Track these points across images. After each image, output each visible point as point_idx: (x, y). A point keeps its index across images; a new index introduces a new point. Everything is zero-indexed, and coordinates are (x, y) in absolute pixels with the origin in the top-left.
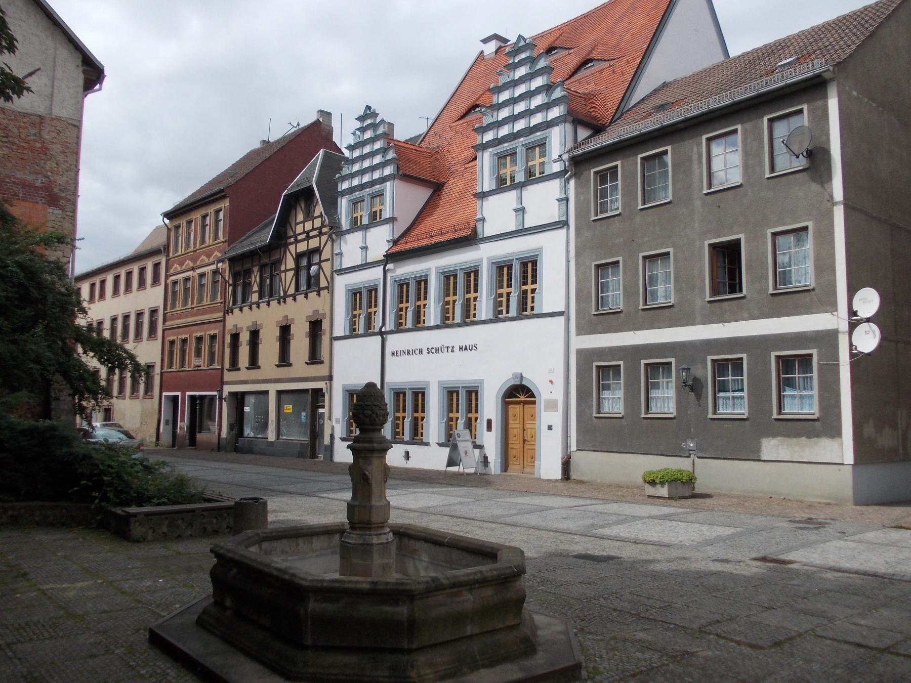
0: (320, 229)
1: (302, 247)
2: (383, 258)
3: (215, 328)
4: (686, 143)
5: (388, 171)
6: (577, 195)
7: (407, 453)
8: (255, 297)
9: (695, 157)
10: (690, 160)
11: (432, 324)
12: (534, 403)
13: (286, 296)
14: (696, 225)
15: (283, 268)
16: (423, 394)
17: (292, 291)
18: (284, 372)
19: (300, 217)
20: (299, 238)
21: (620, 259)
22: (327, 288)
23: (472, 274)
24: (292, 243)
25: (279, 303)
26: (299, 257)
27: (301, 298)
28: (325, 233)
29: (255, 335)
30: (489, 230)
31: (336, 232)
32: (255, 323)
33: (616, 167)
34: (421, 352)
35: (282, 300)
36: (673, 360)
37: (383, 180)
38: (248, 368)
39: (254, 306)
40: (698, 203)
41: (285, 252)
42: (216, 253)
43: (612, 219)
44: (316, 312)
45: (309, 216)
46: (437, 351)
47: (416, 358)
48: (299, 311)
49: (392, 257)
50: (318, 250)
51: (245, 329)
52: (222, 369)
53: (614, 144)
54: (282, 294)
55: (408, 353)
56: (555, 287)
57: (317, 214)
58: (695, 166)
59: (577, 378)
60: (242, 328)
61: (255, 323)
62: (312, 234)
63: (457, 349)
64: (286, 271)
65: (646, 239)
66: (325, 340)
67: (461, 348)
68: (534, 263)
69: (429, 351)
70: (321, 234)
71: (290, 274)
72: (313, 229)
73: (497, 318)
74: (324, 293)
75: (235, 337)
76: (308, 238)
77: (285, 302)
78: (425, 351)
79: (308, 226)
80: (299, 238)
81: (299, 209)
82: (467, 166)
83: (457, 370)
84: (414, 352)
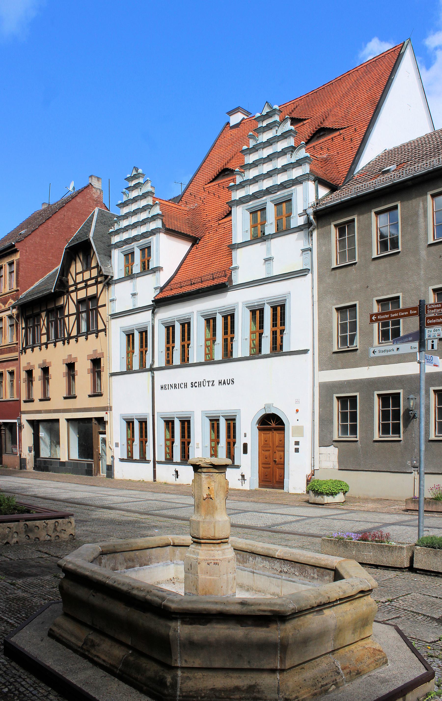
0: (96, 278)
1: (82, 294)
2: (152, 303)
3: (13, 366)
4: (414, 200)
5: (158, 224)
6: (319, 245)
7: (177, 472)
8: (44, 339)
9: (421, 211)
10: (416, 214)
11: (195, 362)
12: (283, 429)
13: (70, 338)
14: (422, 272)
15: (66, 313)
16: (189, 422)
17: (74, 333)
18: (70, 404)
19: (79, 267)
20: (79, 286)
21: (357, 303)
22: (104, 330)
23: (229, 318)
24: (73, 291)
25: (64, 344)
26: (81, 302)
27: (51, 346)
28: (101, 282)
29: (45, 370)
30: (239, 278)
31: (108, 282)
32: (44, 362)
33: (353, 220)
34: (186, 386)
35: (67, 340)
36: (401, 391)
37: (153, 232)
38: (41, 400)
39: (43, 347)
40: (423, 253)
41: (68, 298)
42: (11, 300)
43: (350, 268)
44: (95, 351)
45: (87, 267)
46: (200, 385)
47: (206, 389)
48: (81, 351)
49: (160, 303)
50: (94, 298)
51: (37, 366)
52: (19, 401)
53: (352, 199)
54: (66, 336)
55: (175, 387)
56: (301, 329)
57: (93, 264)
58: (421, 220)
59: (320, 408)
60: (34, 365)
61: (44, 362)
62: (89, 283)
63: (216, 383)
64: (69, 315)
65: (379, 285)
66: (105, 375)
67: (220, 383)
68: (283, 307)
69: (192, 385)
70: (97, 283)
71: (73, 318)
72: (91, 279)
73: (256, 353)
74: (101, 334)
75: (30, 373)
76: (87, 286)
77: (68, 343)
78: (189, 385)
79: (87, 275)
80: (79, 286)
81: (78, 260)
82: (220, 222)
83: (220, 402)
84: (180, 385)
